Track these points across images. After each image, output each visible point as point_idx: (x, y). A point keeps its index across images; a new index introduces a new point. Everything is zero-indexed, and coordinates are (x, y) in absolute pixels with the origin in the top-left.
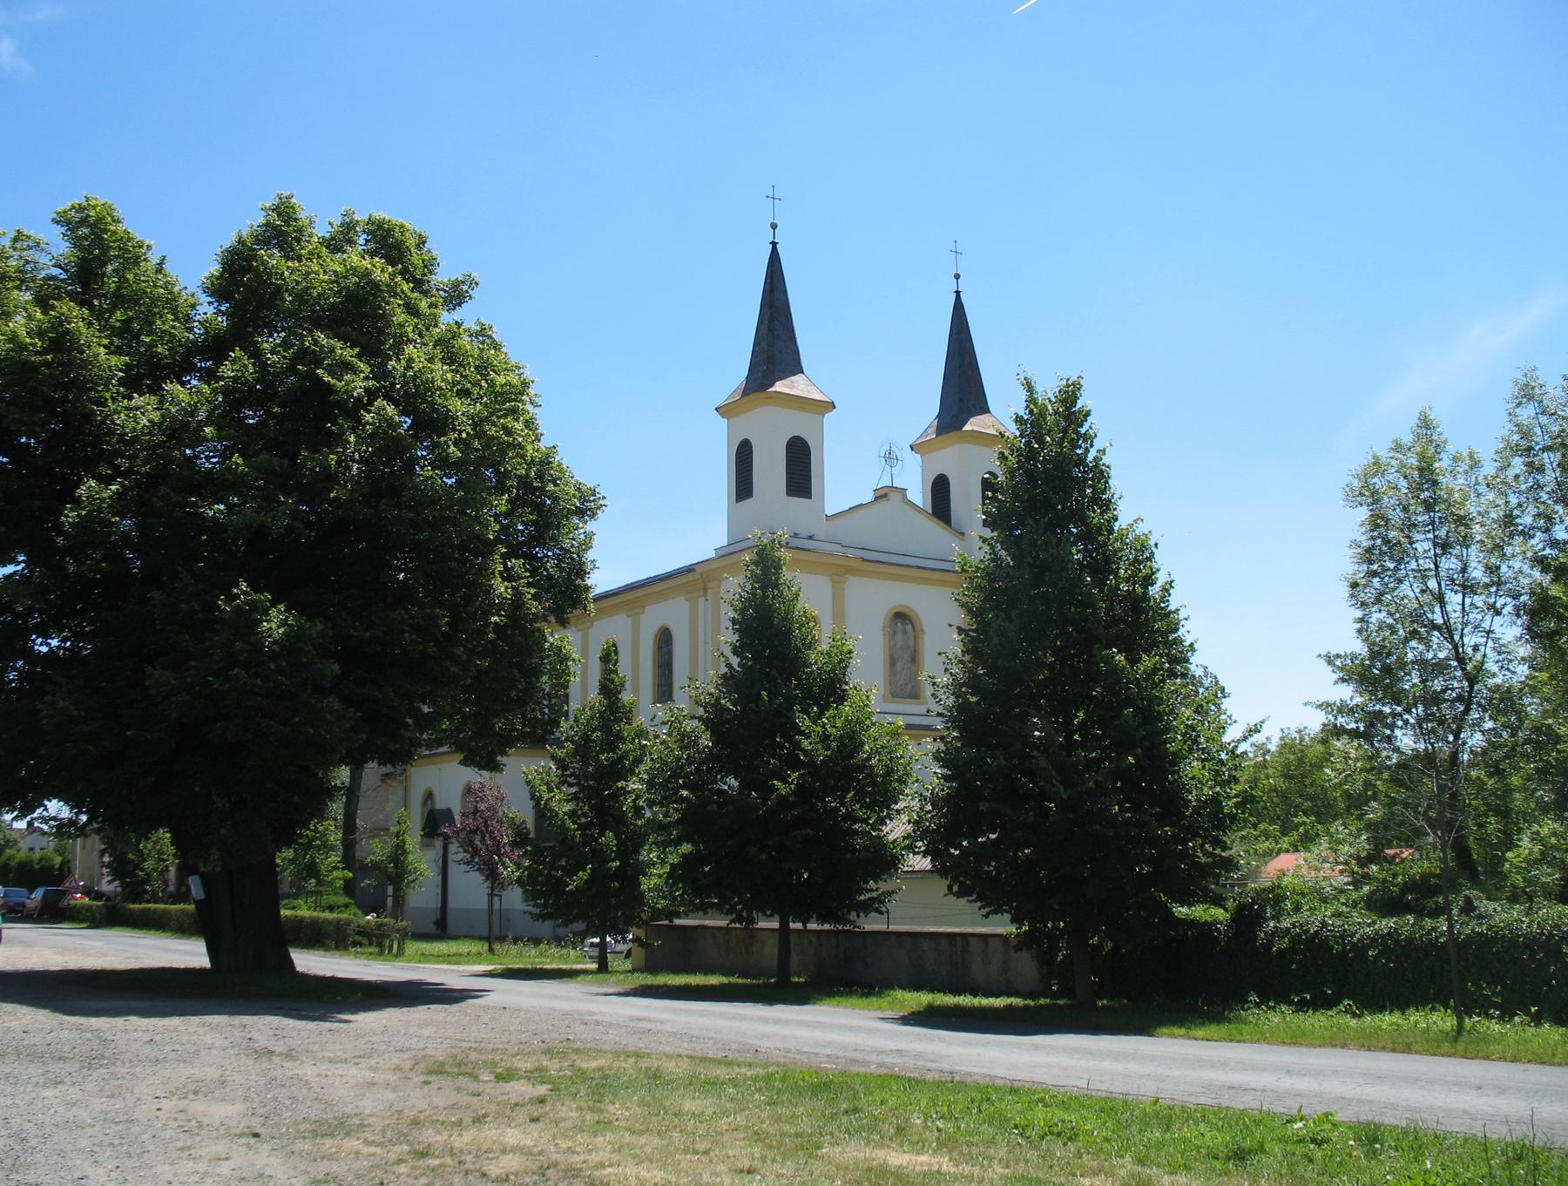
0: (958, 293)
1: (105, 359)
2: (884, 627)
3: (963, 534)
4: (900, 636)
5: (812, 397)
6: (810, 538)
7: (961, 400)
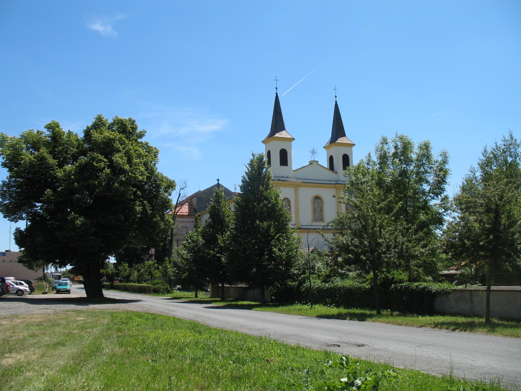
0: (336, 102)
1: (52, 161)
2: (311, 201)
3: (337, 173)
4: (317, 203)
5: (287, 137)
6: (287, 177)
7: (337, 133)
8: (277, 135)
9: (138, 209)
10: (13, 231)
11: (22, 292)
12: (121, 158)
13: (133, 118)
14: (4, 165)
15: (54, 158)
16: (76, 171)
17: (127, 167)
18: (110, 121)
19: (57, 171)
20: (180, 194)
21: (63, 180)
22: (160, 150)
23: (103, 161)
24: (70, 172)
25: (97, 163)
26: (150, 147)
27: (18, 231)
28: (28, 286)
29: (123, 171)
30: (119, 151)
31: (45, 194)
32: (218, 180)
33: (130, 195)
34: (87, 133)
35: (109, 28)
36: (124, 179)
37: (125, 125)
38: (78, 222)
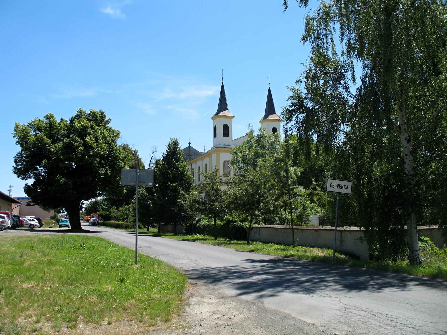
0: (269, 87)
1: (47, 141)
6: (228, 145)
7: (268, 112)
8: (221, 114)
9: (102, 172)
10: (24, 186)
11: (33, 226)
12: (91, 139)
13: (103, 110)
14: (18, 143)
15: (49, 138)
16: (63, 148)
17: (94, 145)
18: (88, 112)
19: (51, 147)
20: (152, 156)
21: (55, 153)
22: (338, 28)
23: (79, 141)
24: (59, 148)
25: (75, 143)
26: (113, 130)
27: (26, 185)
28: (38, 222)
29: (92, 148)
30: (90, 134)
31: (42, 162)
32: (190, 143)
33: (96, 164)
34: (72, 121)
35: (118, 11)
36: (92, 153)
37: (97, 116)
38: (62, 181)
